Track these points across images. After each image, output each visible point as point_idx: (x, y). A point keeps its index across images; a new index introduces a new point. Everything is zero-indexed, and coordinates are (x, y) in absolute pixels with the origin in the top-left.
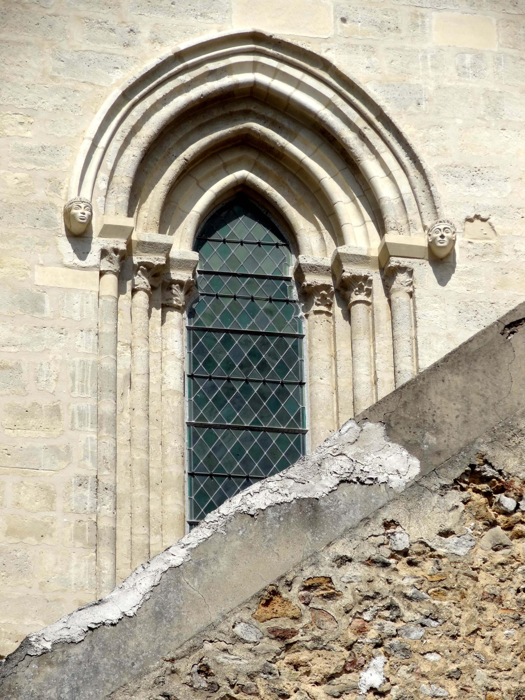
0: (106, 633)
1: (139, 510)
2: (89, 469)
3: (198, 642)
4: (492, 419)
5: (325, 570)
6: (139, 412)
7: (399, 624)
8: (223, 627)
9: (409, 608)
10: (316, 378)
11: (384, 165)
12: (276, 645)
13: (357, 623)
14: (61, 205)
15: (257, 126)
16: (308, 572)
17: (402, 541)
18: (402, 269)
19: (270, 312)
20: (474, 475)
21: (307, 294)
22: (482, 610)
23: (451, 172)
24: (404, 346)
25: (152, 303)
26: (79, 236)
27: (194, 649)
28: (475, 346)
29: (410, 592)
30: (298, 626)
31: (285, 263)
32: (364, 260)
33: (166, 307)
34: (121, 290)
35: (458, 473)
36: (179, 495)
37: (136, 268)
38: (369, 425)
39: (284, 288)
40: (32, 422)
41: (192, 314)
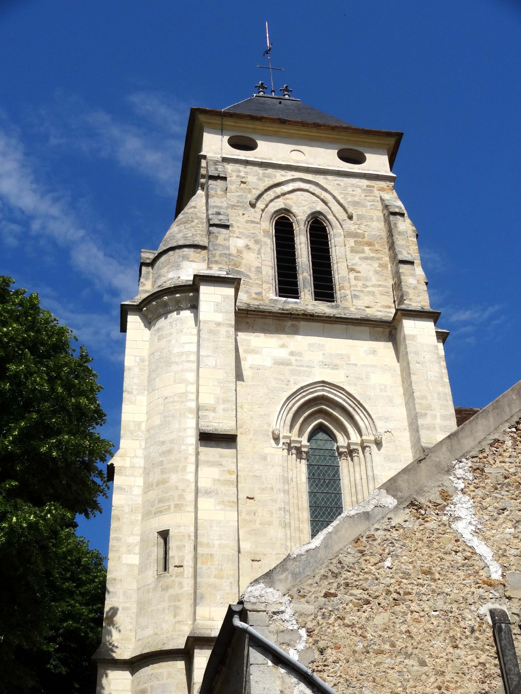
0: (311, 552)
1: (296, 517)
2: (282, 505)
3: (337, 554)
4: (416, 488)
6: (295, 489)
7: (394, 548)
8: (345, 549)
9: (397, 543)
10: (344, 478)
11: (361, 417)
12: (360, 555)
13: (382, 548)
14: (271, 430)
15: (324, 407)
16: (368, 533)
17: (393, 524)
18: (368, 446)
19: (330, 459)
20: (412, 504)
21: (340, 454)
22: (418, 543)
23: (380, 418)
24: (369, 469)
25: (297, 458)
26: (276, 439)
27: (337, 556)
28: (410, 467)
29: (397, 538)
30: (366, 549)
31: (333, 445)
32: (356, 444)
33: (301, 458)
34: (289, 454)
35: (408, 504)
36: (307, 512)
37: (292, 448)
38: (382, 490)
39: (333, 453)
40: (265, 492)
41: (308, 461)
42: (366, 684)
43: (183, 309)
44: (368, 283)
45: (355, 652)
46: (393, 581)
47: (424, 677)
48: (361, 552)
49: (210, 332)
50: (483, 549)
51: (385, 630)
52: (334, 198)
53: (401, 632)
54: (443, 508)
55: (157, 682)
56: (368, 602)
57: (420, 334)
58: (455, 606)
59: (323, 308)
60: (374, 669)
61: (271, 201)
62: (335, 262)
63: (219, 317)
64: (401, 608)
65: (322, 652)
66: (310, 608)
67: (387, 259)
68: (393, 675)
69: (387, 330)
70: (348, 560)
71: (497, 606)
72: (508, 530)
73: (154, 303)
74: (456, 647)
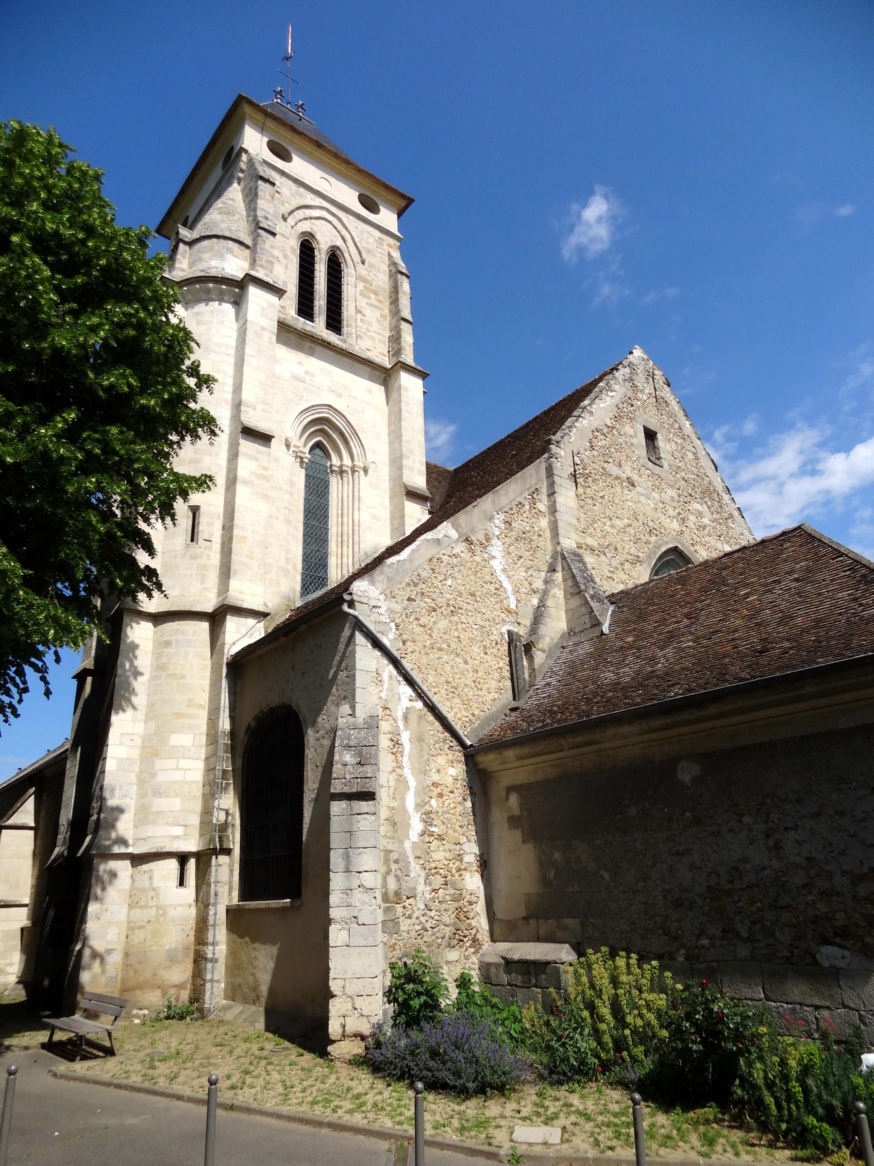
5: (441, 556)
20: (467, 540)
21: (332, 471)
26: (288, 446)
42: (431, 672)
43: (225, 302)
44: (371, 329)
45: (425, 646)
46: (451, 597)
47: (466, 672)
48: (433, 570)
49: (256, 333)
50: (507, 584)
51: (445, 633)
52: (353, 238)
53: (454, 637)
54: (485, 548)
55: (183, 637)
56: (435, 610)
57: (411, 387)
58: (488, 623)
59: (331, 337)
60: (437, 662)
61: (300, 221)
62: (345, 299)
63: (264, 322)
64: (455, 619)
65: (404, 643)
66: (398, 608)
67: (388, 311)
68: (447, 667)
69: (384, 376)
70: (424, 574)
71: (511, 628)
72: (522, 574)
73: (197, 286)
74: (486, 653)
